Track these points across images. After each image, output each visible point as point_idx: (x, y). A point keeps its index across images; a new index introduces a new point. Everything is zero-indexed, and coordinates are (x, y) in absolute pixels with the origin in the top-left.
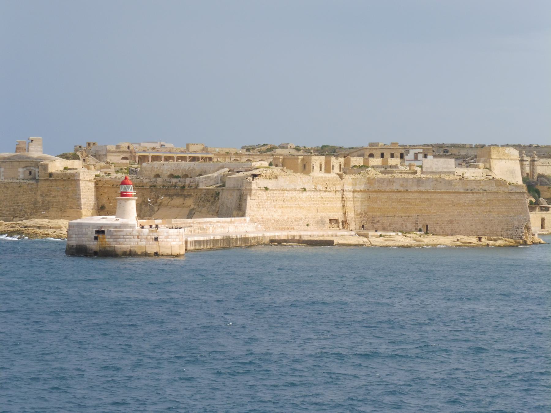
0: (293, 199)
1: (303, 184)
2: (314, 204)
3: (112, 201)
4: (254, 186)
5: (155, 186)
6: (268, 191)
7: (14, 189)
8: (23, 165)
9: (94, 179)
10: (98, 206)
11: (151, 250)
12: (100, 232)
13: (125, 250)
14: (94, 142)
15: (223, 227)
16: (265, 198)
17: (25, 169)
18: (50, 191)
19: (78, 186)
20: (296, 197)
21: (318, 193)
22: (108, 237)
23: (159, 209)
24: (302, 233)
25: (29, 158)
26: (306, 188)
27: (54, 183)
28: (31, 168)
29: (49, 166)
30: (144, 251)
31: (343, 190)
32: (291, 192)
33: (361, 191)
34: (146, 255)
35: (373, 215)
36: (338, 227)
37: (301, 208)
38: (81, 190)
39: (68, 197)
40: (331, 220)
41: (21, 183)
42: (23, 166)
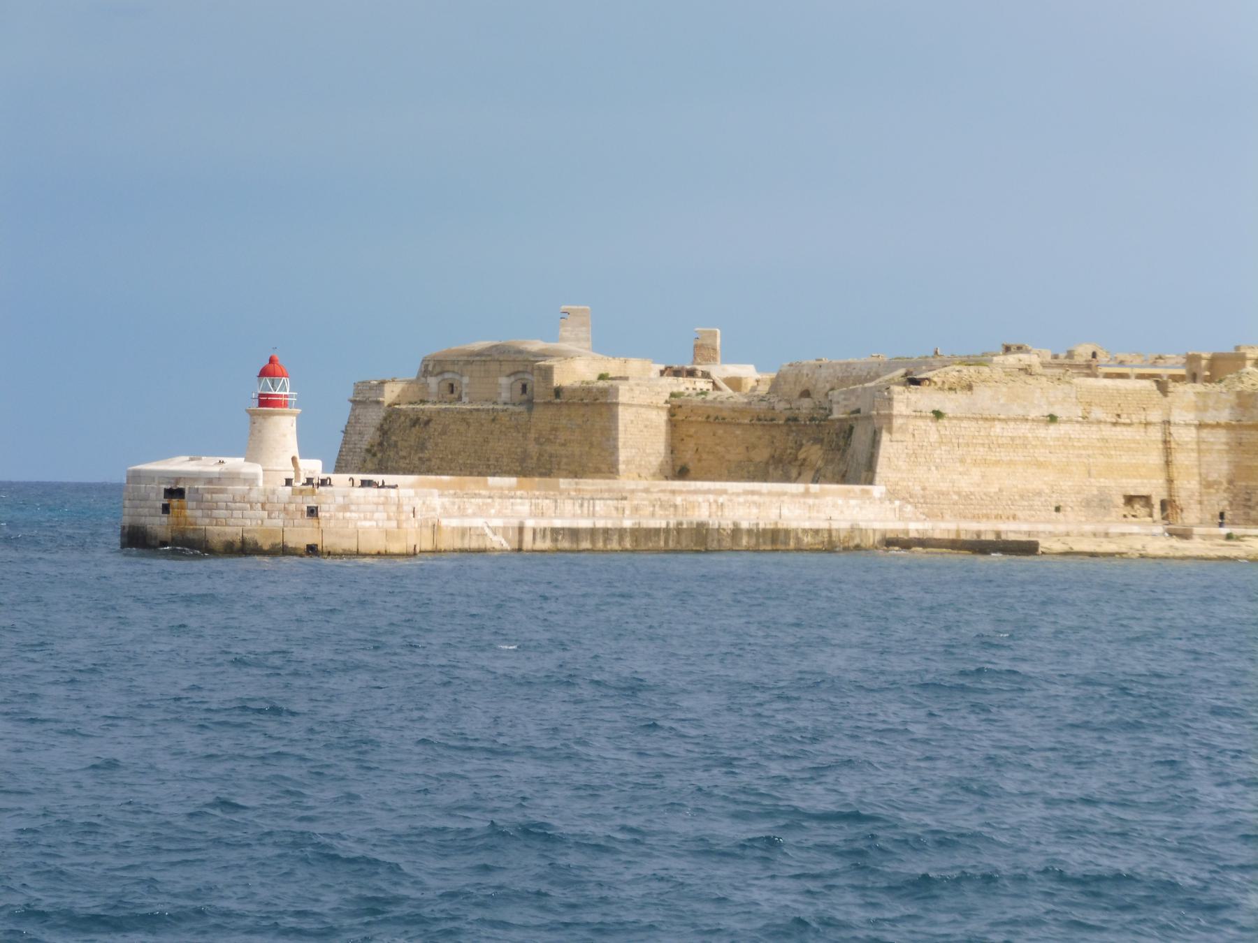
0: (1018, 442)
1: (1051, 404)
2: (1079, 456)
3: (705, 456)
4: (899, 408)
5: (795, 419)
6: (944, 422)
7: (482, 425)
8: (508, 368)
9: (666, 402)
10: (673, 469)
11: (301, 535)
12: (175, 493)
13: (229, 538)
14: (1019, 343)
15: (758, 505)
16: (934, 437)
17: (512, 379)
18: (556, 429)
19: (614, 418)
20: (1026, 438)
21: (1094, 428)
22: (192, 504)
23: (800, 474)
24: (1002, 527)
25: (520, 352)
26: (1057, 414)
27: (565, 411)
28: (527, 376)
29: (556, 371)
30: (279, 540)
31: (1167, 423)
32: (1012, 424)
33: (1218, 425)
34: (283, 551)
35: (1247, 487)
36: (1151, 515)
37: (1039, 465)
38: (621, 428)
39: (591, 445)
40: (1130, 500)
41: (497, 411)
42: (508, 372)
